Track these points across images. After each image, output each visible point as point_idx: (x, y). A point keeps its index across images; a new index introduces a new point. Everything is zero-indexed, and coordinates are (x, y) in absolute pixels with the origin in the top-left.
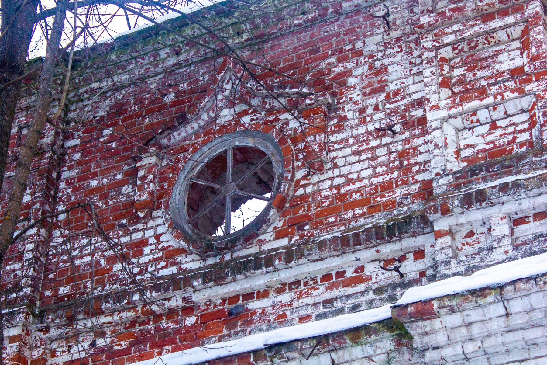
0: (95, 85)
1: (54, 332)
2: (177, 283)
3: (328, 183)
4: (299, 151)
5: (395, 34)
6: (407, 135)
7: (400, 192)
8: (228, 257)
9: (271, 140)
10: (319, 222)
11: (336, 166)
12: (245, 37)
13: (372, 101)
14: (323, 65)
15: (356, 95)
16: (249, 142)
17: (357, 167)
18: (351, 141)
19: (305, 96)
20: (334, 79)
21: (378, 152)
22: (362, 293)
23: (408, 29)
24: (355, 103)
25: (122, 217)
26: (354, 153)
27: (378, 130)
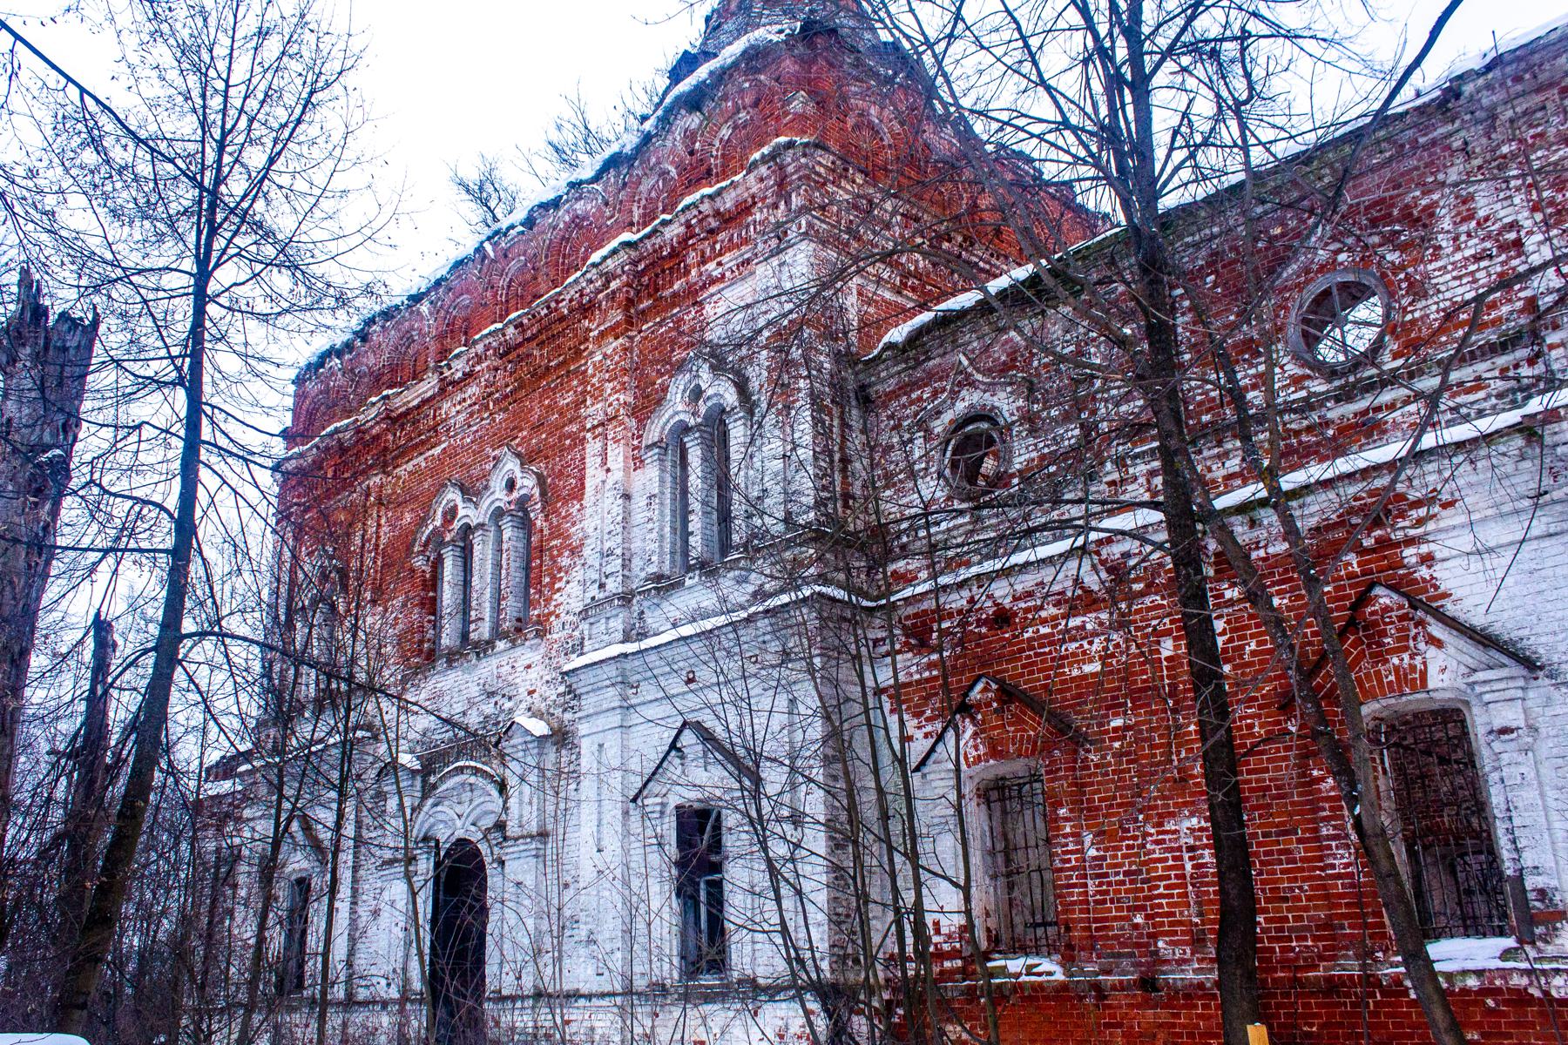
0: (1189, 239)
1: (1206, 453)
2: (1307, 406)
3: (1434, 308)
4: (1401, 281)
5: (1477, 162)
6: (1504, 257)
7: (1505, 309)
8: (1352, 379)
9: (1373, 275)
10: (1431, 340)
11: (1439, 291)
12: (1326, 180)
13: (1464, 228)
14: (1408, 199)
15: (1446, 224)
16: (1351, 278)
17: (1460, 290)
18: (1450, 267)
19: (1399, 233)
20: (1423, 210)
21: (1478, 275)
22: (1485, 399)
23: (1488, 157)
24: (1448, 232)
25: (1243, 352)
26: (1454, 278)
27: (1474, 256)
